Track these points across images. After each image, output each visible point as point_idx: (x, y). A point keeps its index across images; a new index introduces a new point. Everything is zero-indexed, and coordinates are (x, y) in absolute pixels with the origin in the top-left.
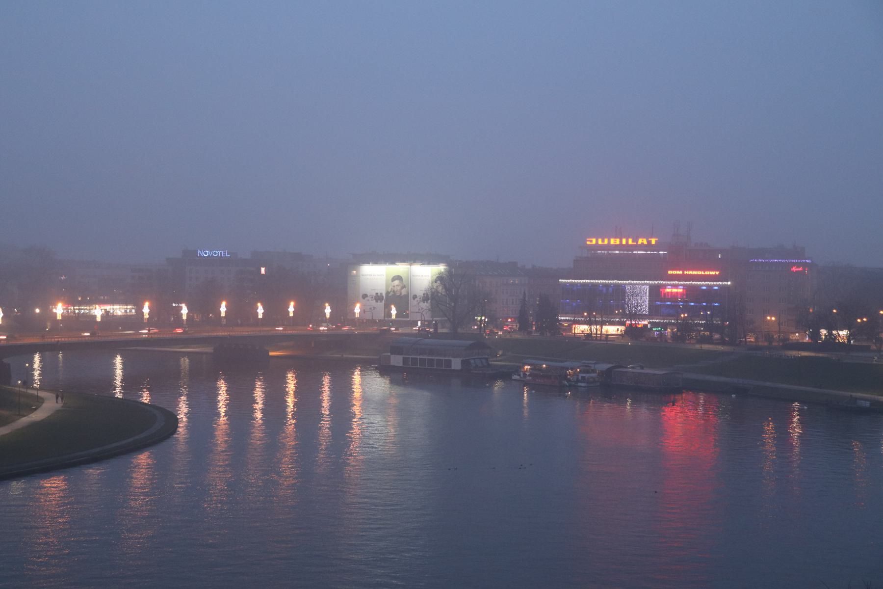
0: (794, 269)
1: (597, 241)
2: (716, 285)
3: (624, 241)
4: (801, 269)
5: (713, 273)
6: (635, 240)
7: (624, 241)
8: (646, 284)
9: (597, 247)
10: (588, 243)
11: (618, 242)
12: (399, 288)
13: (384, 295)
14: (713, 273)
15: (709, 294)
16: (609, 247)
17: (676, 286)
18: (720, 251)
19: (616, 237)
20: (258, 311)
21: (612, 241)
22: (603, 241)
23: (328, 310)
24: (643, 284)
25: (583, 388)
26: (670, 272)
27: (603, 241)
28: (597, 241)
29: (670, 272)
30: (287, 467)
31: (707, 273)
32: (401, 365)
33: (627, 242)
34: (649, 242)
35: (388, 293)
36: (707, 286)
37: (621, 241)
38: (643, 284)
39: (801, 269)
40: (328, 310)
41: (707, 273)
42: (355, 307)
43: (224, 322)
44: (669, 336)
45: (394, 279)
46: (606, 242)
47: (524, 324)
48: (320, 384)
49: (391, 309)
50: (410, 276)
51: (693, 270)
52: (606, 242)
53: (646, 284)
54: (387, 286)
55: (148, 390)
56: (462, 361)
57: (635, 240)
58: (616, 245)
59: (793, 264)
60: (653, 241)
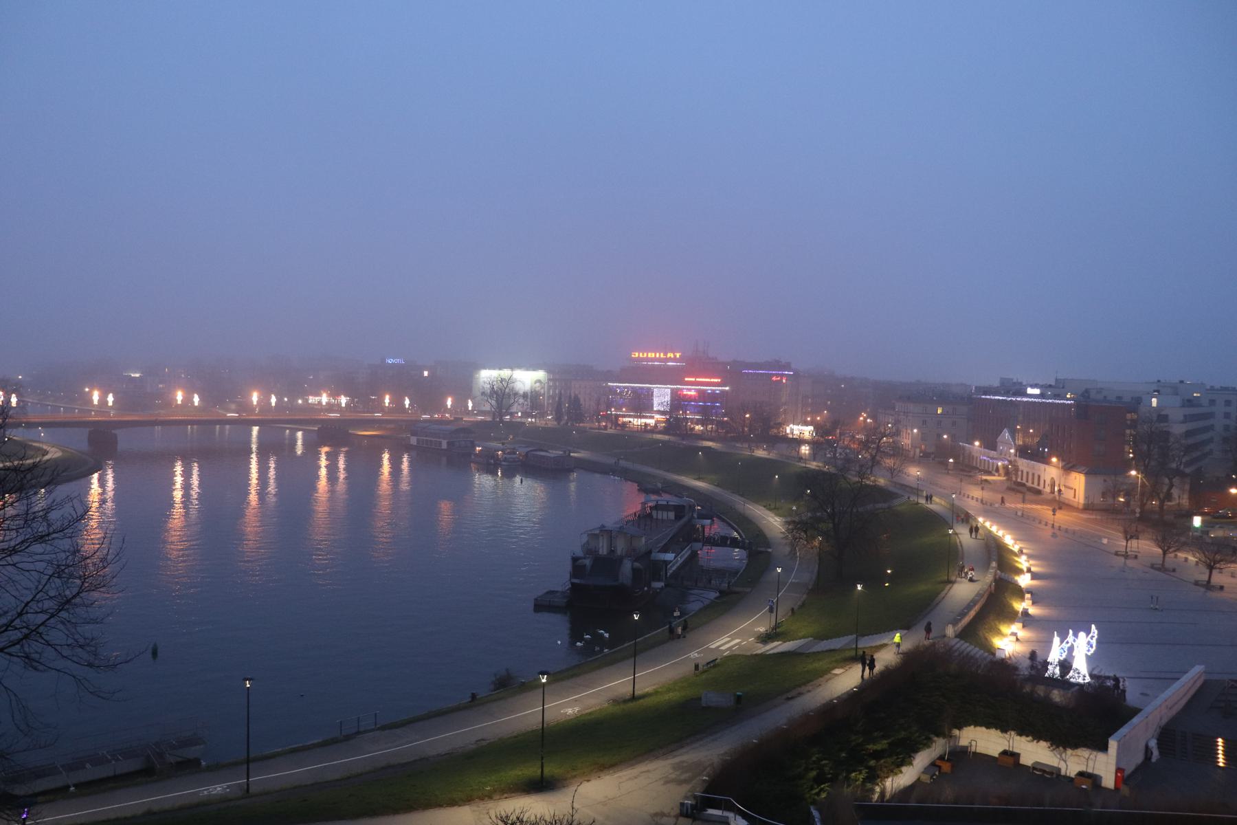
0: (774, 379)
1: (639, 355)
2: (718, 389)
3: (658, 355)
4: (779, 379)
5: (716, 380)
6: (666, 354)
7: (658, 355)
8: (668, 388)
9: (639, 359)
10: (633, 356)
11: (653, 355)
12: (539, 388)
13: (529, 394)
14: (716, 380)
15: (713, 397)
16: (648, 359)
17: (690, 390)
18: (728, 364)
19: (651, 352)
20: (406, 403)
21: (649, 355)
22: (643, 355)
23: (449, 402)
24: (666, 388)
25: (41, 512)
26: (686, 379)
27: (643, 355)
28: (639, 355)
29: (686, 379)
30: (198, 542)
31: (712, 380)
32: (415, 444)
33: (660, 356)
34: (675, 356)
35: (531, 390)
36: (711, 390)
37: (655, 355)
38: (666, 388)
39: (779, 379)
40: (449, 402)
41: (712, 380)
42: (252, 396)
43: (345, 409)
44: (287, 437)
45: (536, 382)
46: (645, 355)
47: (558, 418)
48: (381, 459)
49: (270, 398)
50: (510, 381)
51: (706, 378)
52: (645, 355)
53: (668, 388)
54: (532, 387)
55: (198, 462)
56: (448, 443)
57: (666, 354)
58: (652, 358)
59: (773, 375)
60: (678, 355)
